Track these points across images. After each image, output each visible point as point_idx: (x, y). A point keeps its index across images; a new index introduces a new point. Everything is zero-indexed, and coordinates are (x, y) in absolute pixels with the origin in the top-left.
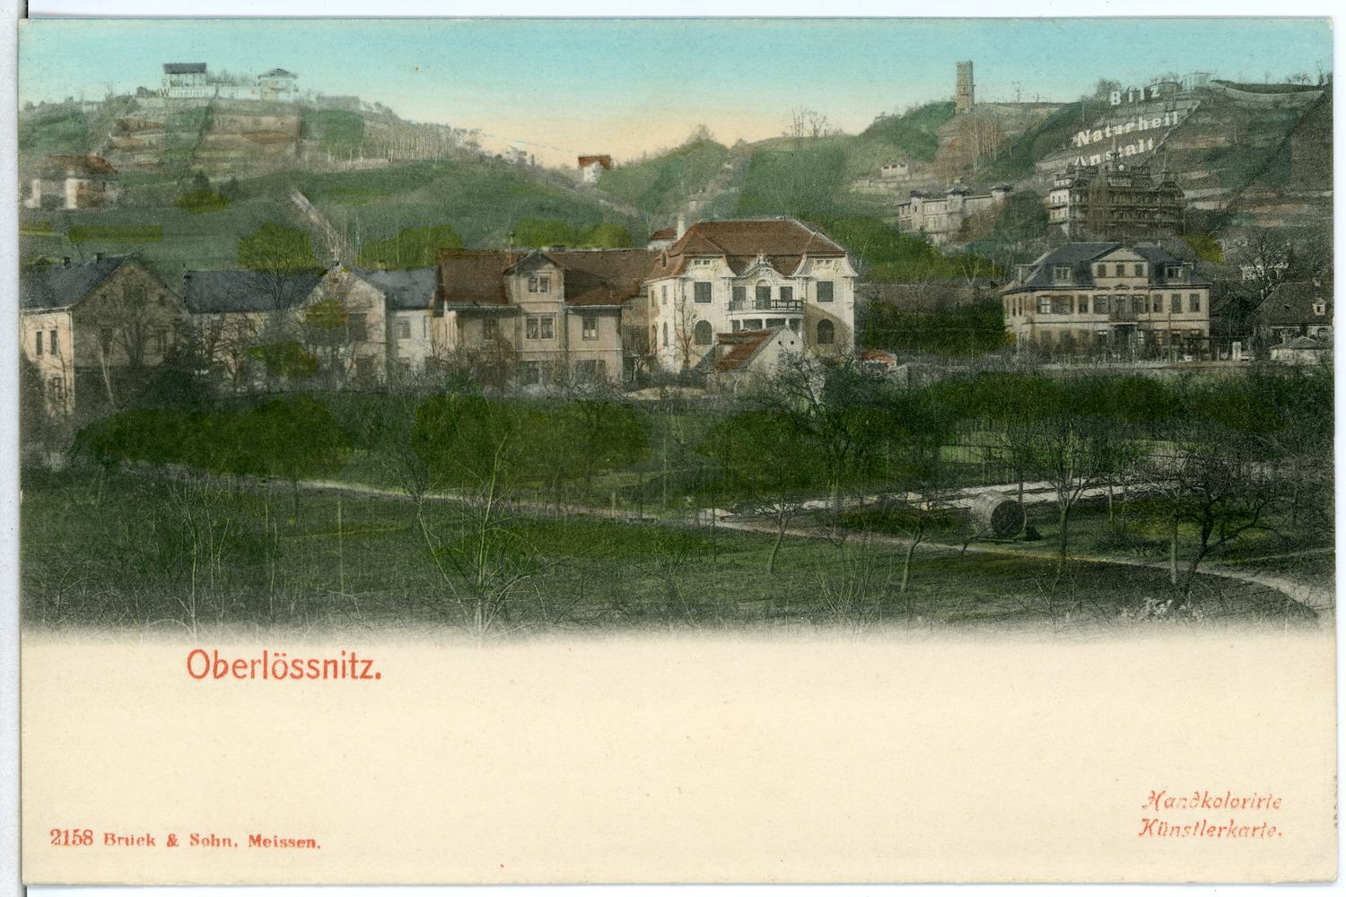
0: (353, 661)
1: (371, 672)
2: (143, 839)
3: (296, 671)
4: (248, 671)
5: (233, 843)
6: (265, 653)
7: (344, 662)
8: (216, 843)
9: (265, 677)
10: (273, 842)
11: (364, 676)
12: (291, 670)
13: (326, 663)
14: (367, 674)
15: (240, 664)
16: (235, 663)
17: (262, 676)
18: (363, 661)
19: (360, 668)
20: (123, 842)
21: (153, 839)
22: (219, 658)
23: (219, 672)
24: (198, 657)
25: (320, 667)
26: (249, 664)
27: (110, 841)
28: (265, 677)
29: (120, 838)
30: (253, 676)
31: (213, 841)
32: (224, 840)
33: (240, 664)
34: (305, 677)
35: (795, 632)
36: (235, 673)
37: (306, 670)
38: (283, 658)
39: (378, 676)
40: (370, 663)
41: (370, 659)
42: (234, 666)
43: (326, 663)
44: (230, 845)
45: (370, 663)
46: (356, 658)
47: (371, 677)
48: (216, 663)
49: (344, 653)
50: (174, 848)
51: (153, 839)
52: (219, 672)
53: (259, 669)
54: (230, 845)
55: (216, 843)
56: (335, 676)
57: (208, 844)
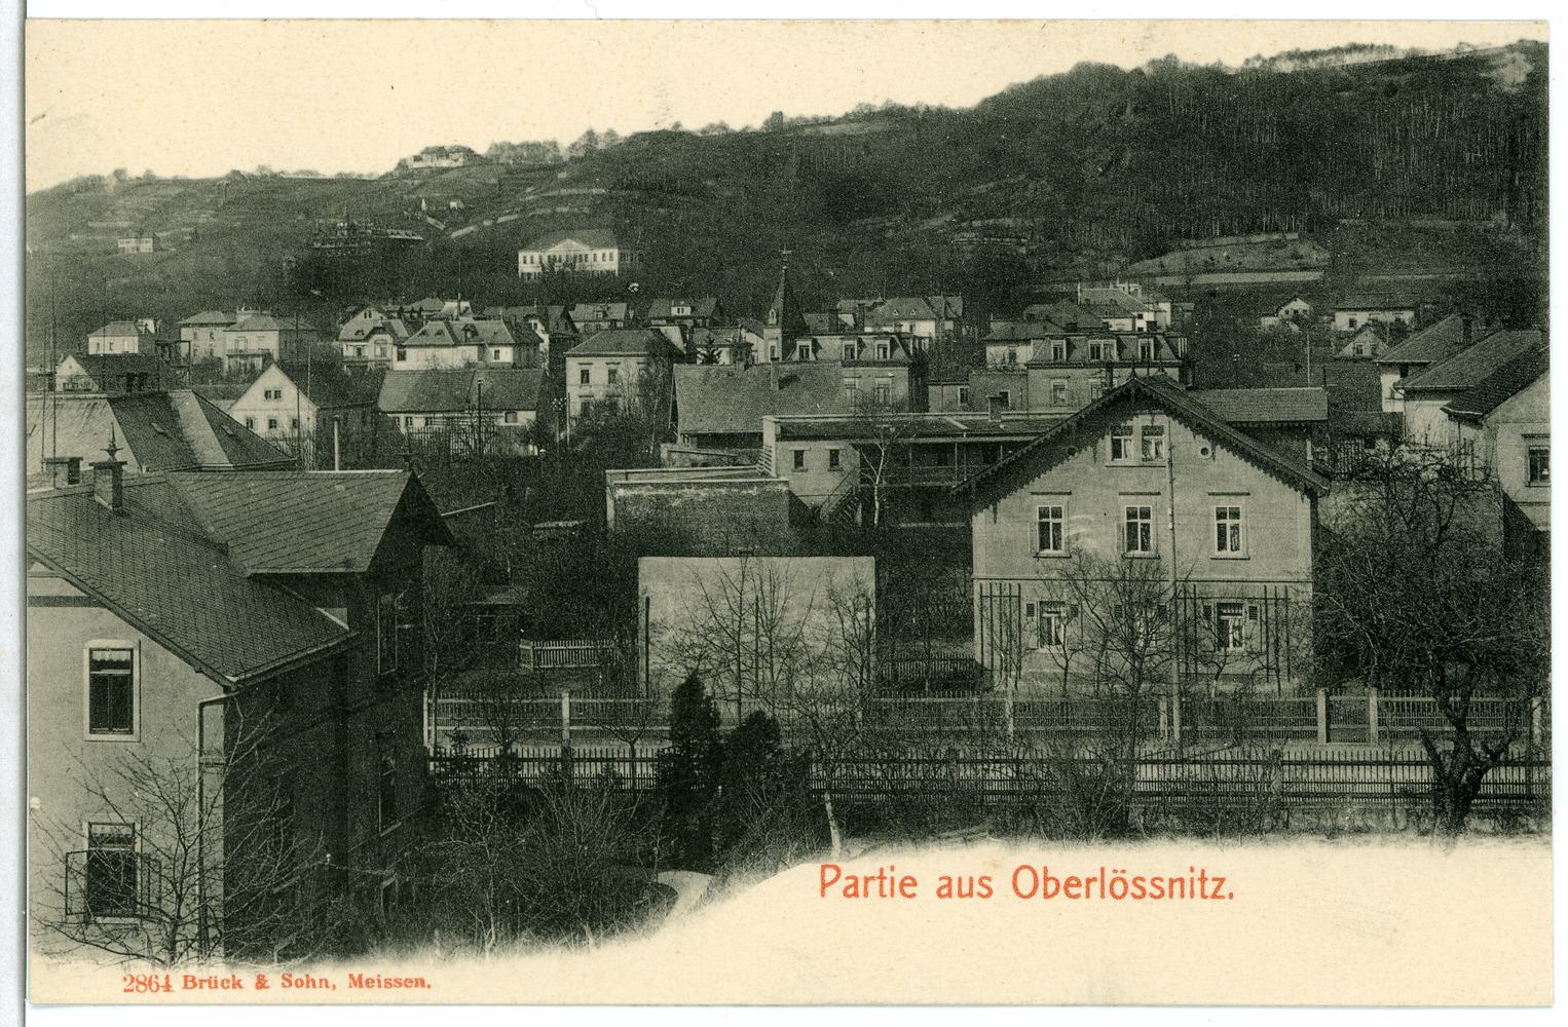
0: (1203, 879)
1: (1223, 891)
2: (228, 981)
3: (1139, 889)
4: (1082, 890)
5: (330, 984)
6: (1103, 870)
7: (1192, 880)
8: (311, 984)
9: (1103, 896)
10: (376, 982)
11: (1214, 896)
12: (1132, 889)
13: (1172, 881)
14: (1219, 894)
15: (909, 881)
16: (903, 880)
17: (820, 893)
18: (1214, 879)
19: (1210, 887)
20: (205, 985)
21: (239, 981)
22: (1049, 875)
23: (1050, 891)
24: (1025, 873)
25: (1165, 885)
26: (1084, 882)
27: (190, 984)
28: (1103, 896)
29: (201, 981)
30: (1088, 896)
31: (308, 983)
32: (321, 981)
33: (909, 881)
34: (1147, 898)
35: (736, 874)
36: (904, 894)
37: (1150, 889)
38: (1122, 875)
39: (1231, 896)
40: (1222, 880)
41: (1222, 876)
42: (902, 884)
43: (1172, 881)
44: (327, 986)
45: (1222, 880)
46: (1206, 876)
47: (1222, 897)
48: (1046, 879)
49: (1192, 870)
50: (263, 991)
51: (239, 981)
52: (1050, 891)
53: (1095, 887)
54: (327, 986)
55: (311, 984)
56: (1182, 896)
57: (302, 985)
